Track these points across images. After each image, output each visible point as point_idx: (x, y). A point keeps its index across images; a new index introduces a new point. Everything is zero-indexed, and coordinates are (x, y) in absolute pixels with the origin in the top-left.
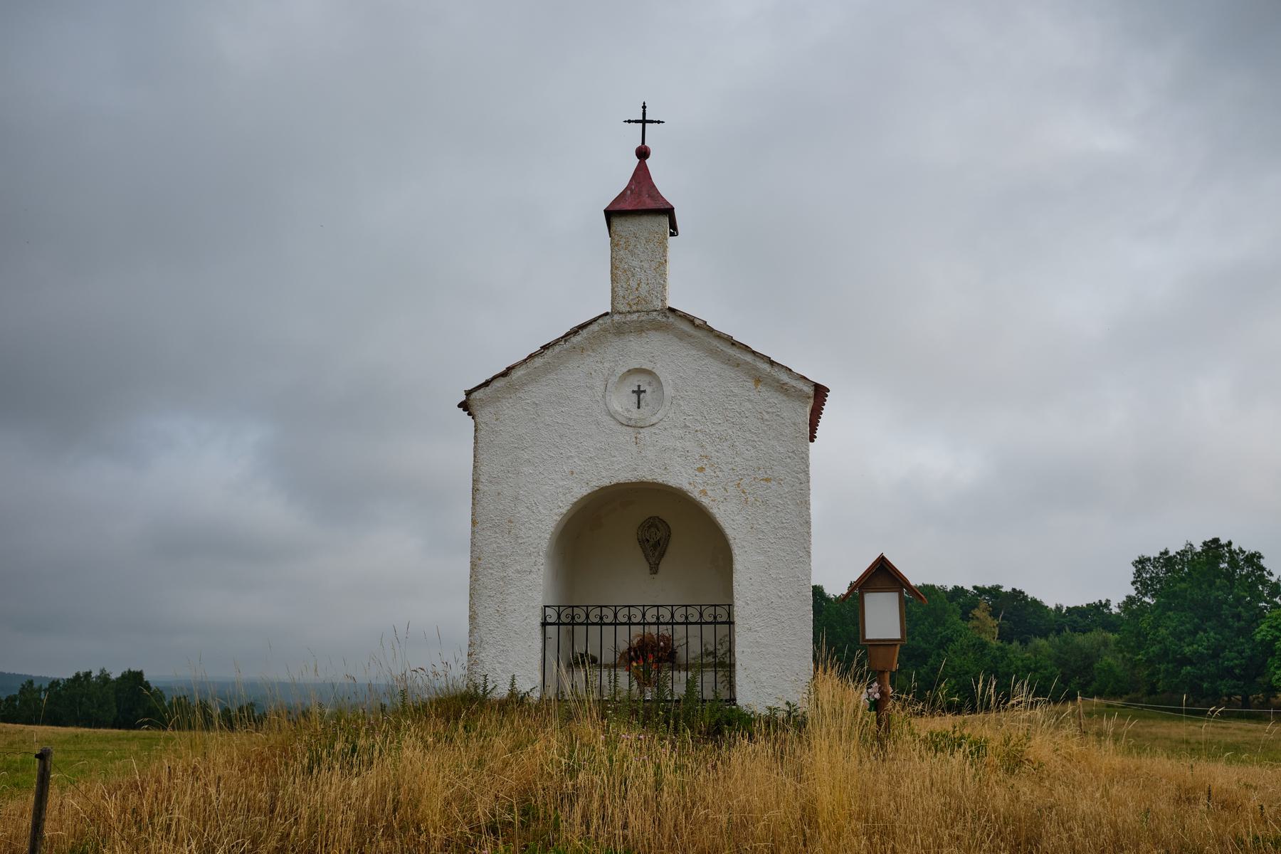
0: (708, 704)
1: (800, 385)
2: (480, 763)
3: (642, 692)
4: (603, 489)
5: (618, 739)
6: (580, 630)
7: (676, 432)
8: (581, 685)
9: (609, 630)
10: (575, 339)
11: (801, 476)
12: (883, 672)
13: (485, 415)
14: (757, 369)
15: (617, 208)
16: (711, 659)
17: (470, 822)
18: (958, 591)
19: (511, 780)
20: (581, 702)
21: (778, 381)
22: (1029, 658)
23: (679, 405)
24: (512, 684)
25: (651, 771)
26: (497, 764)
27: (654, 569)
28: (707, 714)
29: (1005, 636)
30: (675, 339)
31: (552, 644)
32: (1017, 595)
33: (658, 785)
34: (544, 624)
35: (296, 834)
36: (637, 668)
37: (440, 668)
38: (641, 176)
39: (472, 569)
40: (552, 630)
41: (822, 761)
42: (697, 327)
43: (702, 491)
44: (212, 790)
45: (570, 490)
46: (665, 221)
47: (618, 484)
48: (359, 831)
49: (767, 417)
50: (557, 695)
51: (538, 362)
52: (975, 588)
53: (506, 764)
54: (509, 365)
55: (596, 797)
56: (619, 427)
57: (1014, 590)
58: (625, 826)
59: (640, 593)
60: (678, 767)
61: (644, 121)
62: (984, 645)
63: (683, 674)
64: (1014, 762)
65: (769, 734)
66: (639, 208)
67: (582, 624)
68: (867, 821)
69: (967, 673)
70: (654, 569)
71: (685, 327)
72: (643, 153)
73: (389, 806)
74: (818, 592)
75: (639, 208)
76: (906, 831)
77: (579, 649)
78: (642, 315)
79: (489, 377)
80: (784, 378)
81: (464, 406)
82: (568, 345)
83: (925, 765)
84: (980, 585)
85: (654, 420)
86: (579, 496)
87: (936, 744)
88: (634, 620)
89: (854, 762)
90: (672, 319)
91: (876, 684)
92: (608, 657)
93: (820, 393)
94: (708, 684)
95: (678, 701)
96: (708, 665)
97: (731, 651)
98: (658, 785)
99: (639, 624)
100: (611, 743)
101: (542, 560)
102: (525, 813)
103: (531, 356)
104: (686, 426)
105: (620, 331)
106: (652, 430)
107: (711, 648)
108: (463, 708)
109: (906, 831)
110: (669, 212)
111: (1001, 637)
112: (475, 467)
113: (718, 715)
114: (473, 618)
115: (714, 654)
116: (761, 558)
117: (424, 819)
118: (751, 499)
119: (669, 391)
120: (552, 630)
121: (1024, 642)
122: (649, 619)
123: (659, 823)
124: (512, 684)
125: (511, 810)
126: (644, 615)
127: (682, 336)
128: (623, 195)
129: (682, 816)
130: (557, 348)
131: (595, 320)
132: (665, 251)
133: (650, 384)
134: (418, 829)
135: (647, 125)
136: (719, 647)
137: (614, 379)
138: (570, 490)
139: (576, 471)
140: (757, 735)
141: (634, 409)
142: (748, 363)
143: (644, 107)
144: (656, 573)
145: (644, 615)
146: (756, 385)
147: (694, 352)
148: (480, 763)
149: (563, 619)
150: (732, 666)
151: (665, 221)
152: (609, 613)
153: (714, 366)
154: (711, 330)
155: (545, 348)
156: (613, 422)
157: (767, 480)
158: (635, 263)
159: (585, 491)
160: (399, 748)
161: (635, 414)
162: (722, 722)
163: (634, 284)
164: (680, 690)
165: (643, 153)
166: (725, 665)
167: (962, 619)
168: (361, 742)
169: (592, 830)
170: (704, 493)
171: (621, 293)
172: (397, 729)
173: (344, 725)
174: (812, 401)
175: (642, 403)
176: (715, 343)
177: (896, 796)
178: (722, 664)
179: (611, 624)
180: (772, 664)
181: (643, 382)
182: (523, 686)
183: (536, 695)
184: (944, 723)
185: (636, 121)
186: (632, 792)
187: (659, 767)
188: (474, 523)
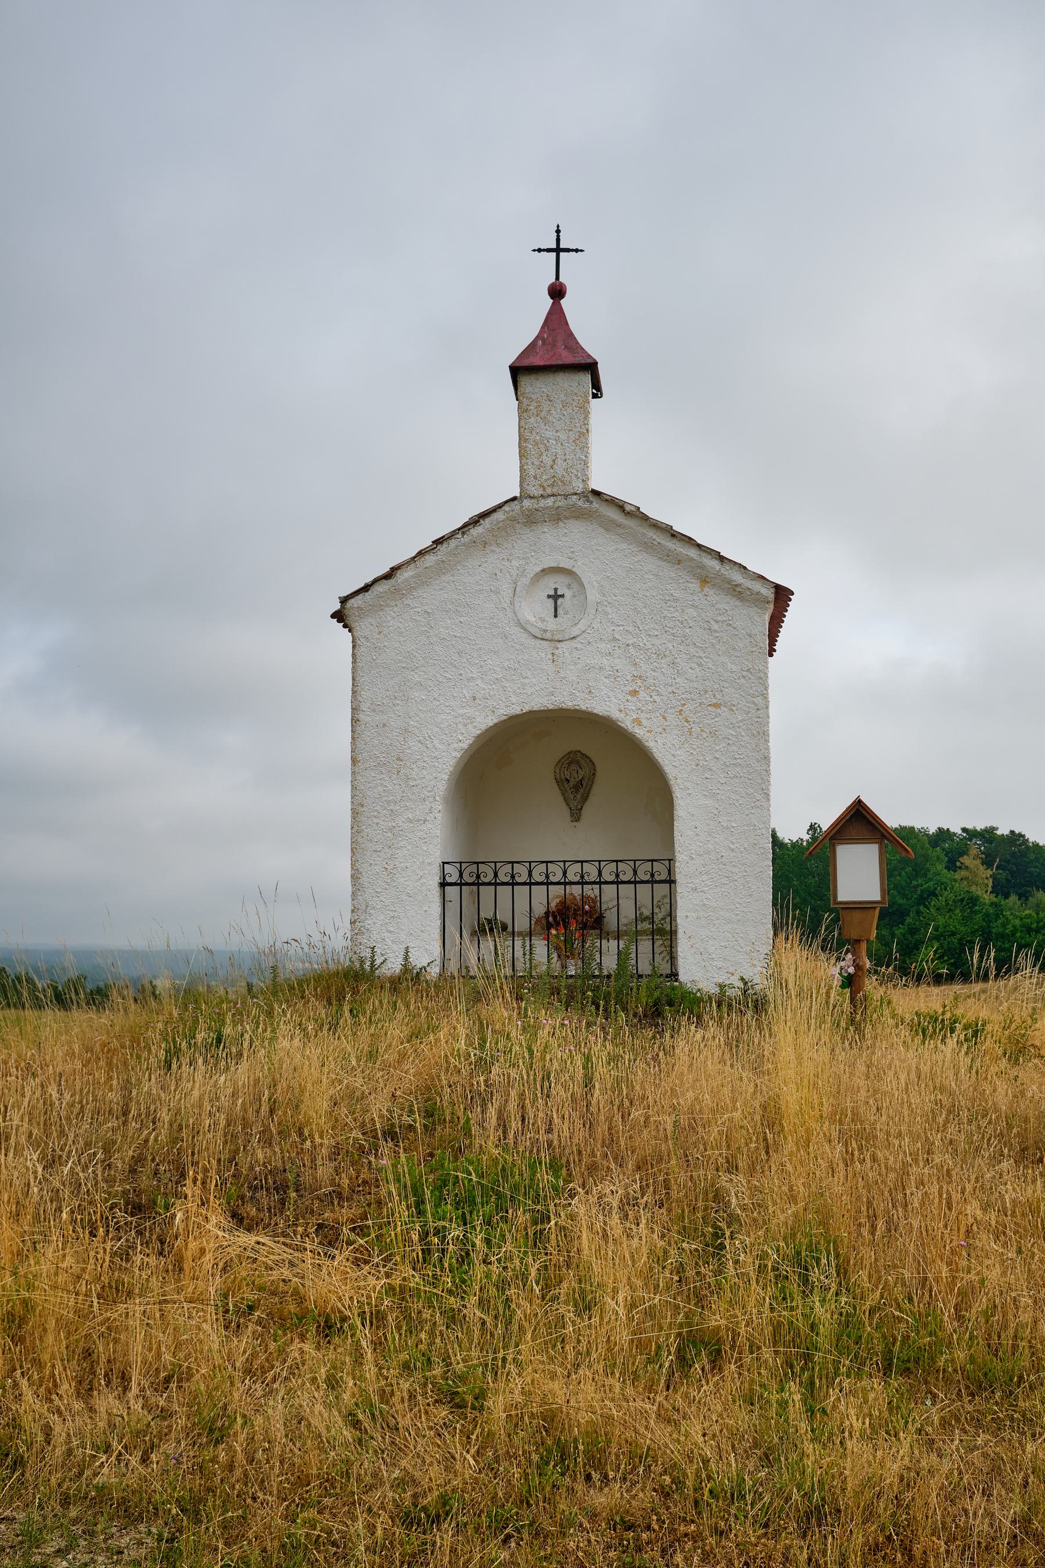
0: (645, 980)
1: (757, 586)
2: (372, 1055)
3: (564, 967)
4: (513, 718)
5: (537, 1027)
6: (487, 892)
7: (602, 646)
8: (489, 957)
9: (522, 891)
10: (476, 531)
11: (759, 700)
12: (858, 941)
13: (365, 627)
14: (702, 567)
15: (526, 362)
16: (646, 925)
17: (363, 1125)
18: (943, 835)
19: (410, 1075)
20: (489, 978)
21: (729, 582)
22: (1029, 916)
23: (607, 613)
24: (406, 958)
25: (579, 1061)
26: (391, 1057)
27: (576, 815)
28: (643, 993)
29: (1000, 889)
30: (602, 530)
31: (453, 908)
32: (1016, 838)
33: (588, 1082)
34: (443, 885)
35: (156, 1140)
36: (557, 936)
37: (316, 937)
38: (556, 320)
39: (354, 818)
40: (452, 892)
41: (787, 1053)
42: (628, 514)
43: (634, 721)
44: (53, 1091)
45: (472, 719)
46: (586, 378)
47: (531, 712)
48: (230, 1137)
49: (715, 626)
50: (460, 971)
51: (430, 560)
52: (964, 830)
53: (403, 1056)
55: (513, 1093)
56: (533, 642)
57: (1012, 832)
58: (549, 1131)
59: (561, 844)
60: (613, 1059)
61: (558, 250)
62: (974, 901)
63: (613, 943)
64: (1018, 1050)
65: (721, 1018)
66: (554, 363)
67: (489, 884)
68: (841, 1123)
69: (953, 934)
70: (576, 815)
71: (613, 514)
72: (557, 292)
73: (265, 1108)
74: (775, 841)
75: (554, 363)
76: (888, 1134)
77: (487, 913)
78: (557, 501)
79: (369, 579)
80: (737, 577)
81: (339, 616)
82: (466, 538)
83: (911, 1054)
84: (970, 826)
85: (575, 632)
86: (484, 727)
87: (930, 1028)
88: (552, 879)
89: (825, 1052)
90: (596, 504)
91: (850, 956)
92: (522, 923)
93: (782, 596)
94: (644, 956)
95: (609, 977)
96: (644, 932)
97: (671, 915)
98: (588, 1082)
99: (558, 883)
100: (530, 1030)
101: (439, 806)
102: (429, 1114)
103: (421, 553)
104: (615, 639)
105: (531, 519)
106: (573, 644)
107: (647, 912)
108: (346, 987)
109: (888, 1134)
110: (591, 367)
111: (995, 891)
112: (354, 692)
113: (657, 994)
114: (355, 877)
115: (651, 919)
117: (308, 1123)
118: (696, 729)
119: (593, 595)
120: (452, 892)
121: (1024, 896)
122: (571, 877)
123: (591, 1126)
124: (406, 958)
125: (411, 1112)
126: (565, 873)
127: (609, 526)
128: (532, 346)
129: (618, 1118)
130: (453, 543)
131: (500, 506)
132: (586, 417)
133: (569, 586)
134: (301, 1133)
135: (562, 254)
136: (656, 910)
137: (525, 581)
138: (472, 719)
139: (478, 696)
140: (706, 1018)
141: (550, 619)
142: (692, 559)
143: (558, 231)
144: (578, 820)
145: (565, 873)
146: (702, 587)
147: (624, 546)
148: (372, 1055)
149: (466, 878)
150: (673, 933)
151: (586, 378)
153: (649, 563)
154: (645, 518)
155: (438, 542)
157: (715, 705)
158: (549, 434)
159: (491, 721)
160: (273, 1039)
161: (551, 624)
162: (663, 1004)
163: (547, 460)
164: (610, 963)
165: (557, 292)
166: (664, 933)
167: (948, 868)
168: (228, 1030)
169: (511, 1136)
170: (638, 722)
171: (532, 472)
172: (270, 1013)
173: (208, 1006)
174: (772, 606)
175: (560, 611)
176: (651, 534)
177: (876, 1092)
178: (661, 932)
179: (524, 884)
180: (722, 929)
181: (560, 583)
182: (419, 960)
183: (435, 971)
184: (931, 999)
185: (549, 250)
186: (558, 1090)
187: (588, 1059)
188: (354, 761)
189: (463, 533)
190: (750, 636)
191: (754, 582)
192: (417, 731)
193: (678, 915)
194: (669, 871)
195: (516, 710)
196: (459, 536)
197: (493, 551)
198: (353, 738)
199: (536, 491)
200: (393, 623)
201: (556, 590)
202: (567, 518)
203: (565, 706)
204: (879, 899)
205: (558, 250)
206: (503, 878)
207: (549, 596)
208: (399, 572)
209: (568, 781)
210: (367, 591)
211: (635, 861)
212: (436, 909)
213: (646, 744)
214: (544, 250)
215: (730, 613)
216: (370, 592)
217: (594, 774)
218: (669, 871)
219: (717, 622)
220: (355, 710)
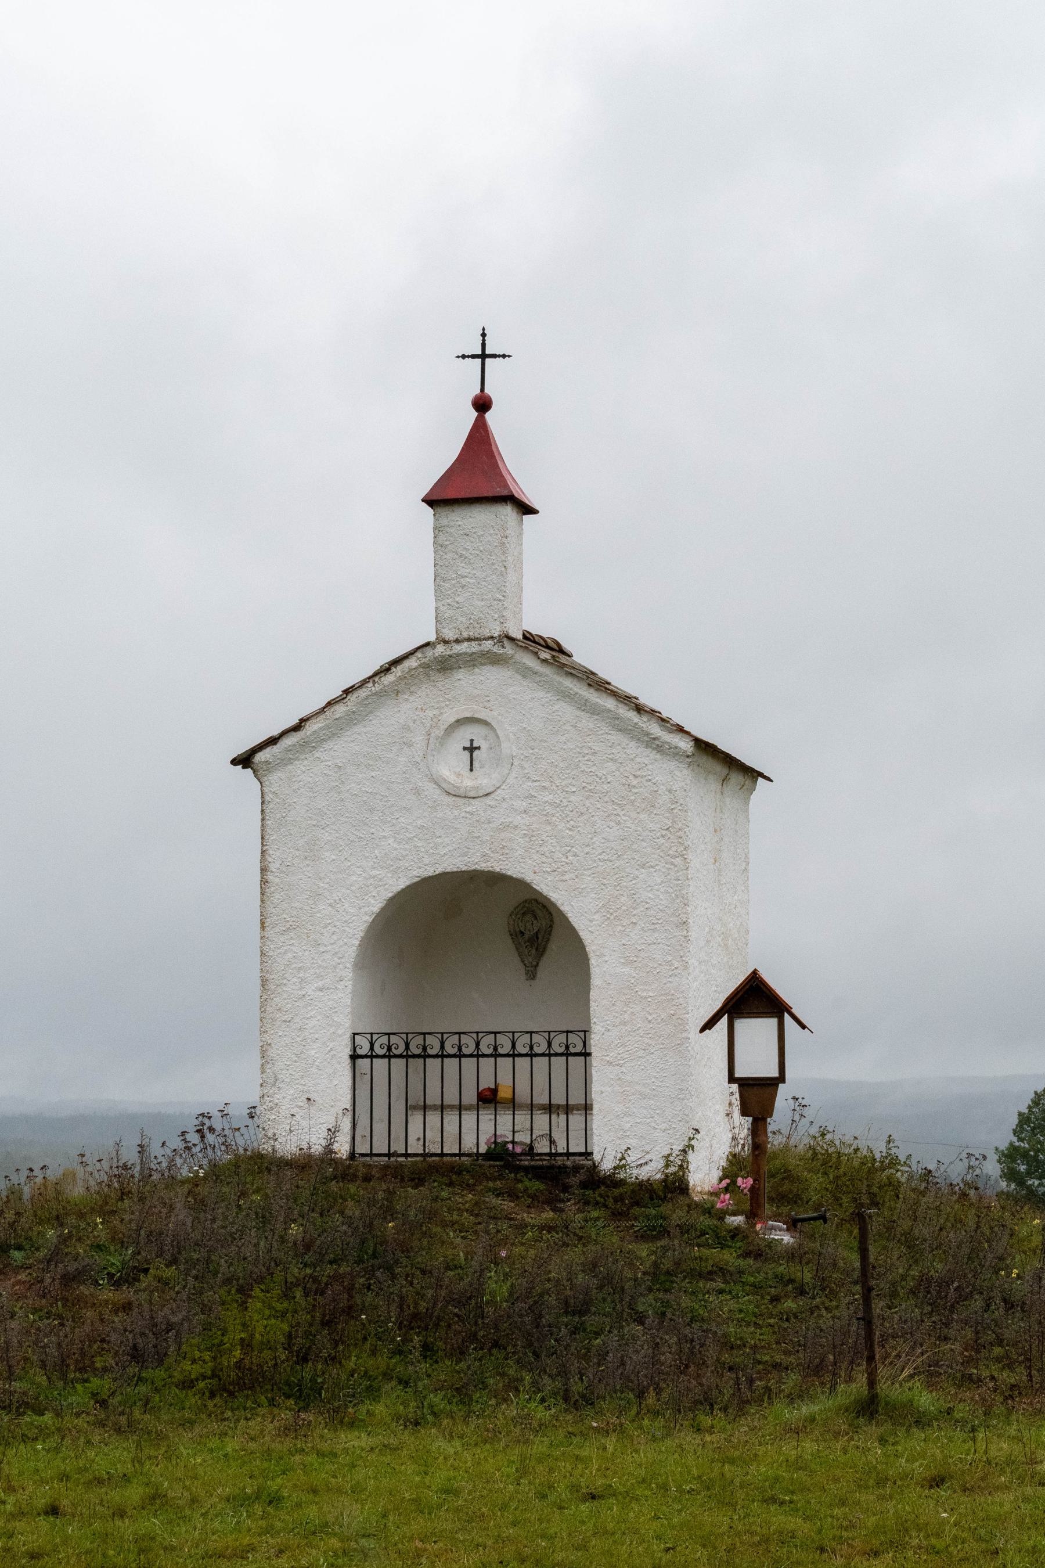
9: (469, 1064)
21: (648, 734)
27: (532, 974)
30: (519, 677)
34: (354, 1057)
38: (479, 444)
40: (364, 1064)
49: (635, 782)
51: (340, 710)
54: (303, 714)
61: (483, 356)
66: (475, 483)
70: (532, 974)
72: (482, 404)
75: (475, 483)
79: (275, 732)
101: (348, 974)
103: (329, 704)
106: (488, 801)
116: (627, 970)
119: (508, 748)
126: (478, 1044)
131: (412, 653)
133: (485, 738)
142: (609, 711)
145: (478, 1044)
147: (541, 694)
152: (434, 1043)
155: (347, 692)
156: (438, 791)
159: (403, 883)
165: (482, 404)
175: (476, 764)
179: (507, 1055)
185: (474, 356)
189: (374, 682)
190: (670, 791)
191: (672, 735)
192: (327, 894)
193: (593, 1089)
194: (585, 1043)
195: (430, 872)
196: (370, 685)
197: (407, 700)
198: (262, 901)
199: (449, 634)
200: (300, 777)
201: (472, 741)
202: (482, 664)
203: (478, 868)
204: (736, 1076)
205: (483, 356)
206: (449, 1049)
207: (465, 749)
208: (308, 723)
209: (522, 932)
210: (275, 744)
211: (549, 1032)
212: (596, 1088)
213: (562, 908)
214: (468, 357)
215: (650, 767)
216: (278, 745)
217: (551, 926)
218: (585, 1043)
219: (636, 777)
220: (264, 870)
